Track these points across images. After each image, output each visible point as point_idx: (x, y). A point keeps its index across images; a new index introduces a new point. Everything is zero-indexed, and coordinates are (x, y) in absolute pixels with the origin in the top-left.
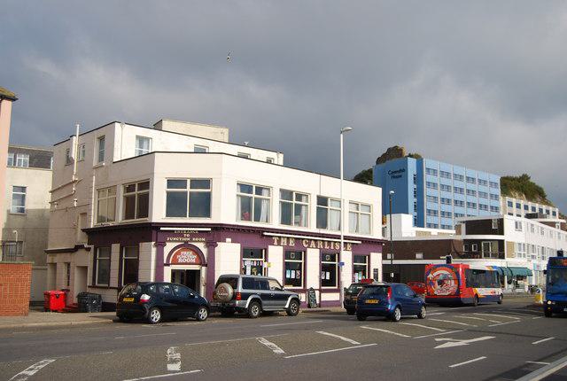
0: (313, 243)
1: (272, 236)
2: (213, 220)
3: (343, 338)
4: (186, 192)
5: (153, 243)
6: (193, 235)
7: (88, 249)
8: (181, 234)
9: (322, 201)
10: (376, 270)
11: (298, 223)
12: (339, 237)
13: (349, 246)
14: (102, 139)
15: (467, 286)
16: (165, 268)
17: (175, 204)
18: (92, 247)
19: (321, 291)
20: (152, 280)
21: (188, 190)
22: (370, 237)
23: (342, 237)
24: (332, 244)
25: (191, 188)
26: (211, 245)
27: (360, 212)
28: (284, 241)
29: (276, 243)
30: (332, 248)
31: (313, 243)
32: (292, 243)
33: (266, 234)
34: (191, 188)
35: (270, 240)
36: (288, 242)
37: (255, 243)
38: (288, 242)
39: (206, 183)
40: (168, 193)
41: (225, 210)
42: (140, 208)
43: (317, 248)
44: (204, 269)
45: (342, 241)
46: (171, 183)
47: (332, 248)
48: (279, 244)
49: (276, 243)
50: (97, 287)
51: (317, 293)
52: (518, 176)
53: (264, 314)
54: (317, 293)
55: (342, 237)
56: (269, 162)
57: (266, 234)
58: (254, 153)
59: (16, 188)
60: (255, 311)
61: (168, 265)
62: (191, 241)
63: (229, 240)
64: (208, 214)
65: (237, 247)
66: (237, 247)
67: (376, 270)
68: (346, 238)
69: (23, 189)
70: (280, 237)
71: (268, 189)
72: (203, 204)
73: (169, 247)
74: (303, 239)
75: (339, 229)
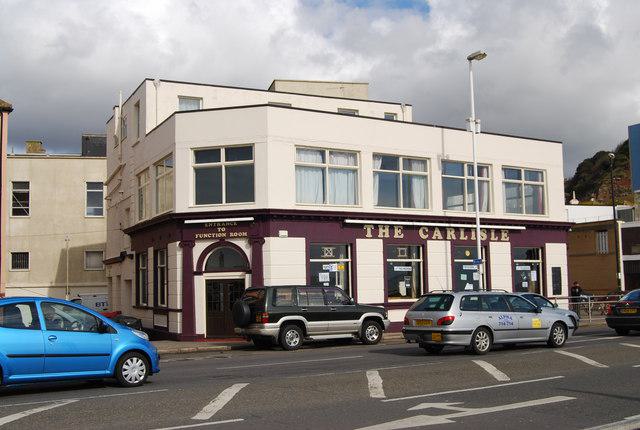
0: (437, 233)
1: (362, 225)
2: (258, 204)
4: (463, 180)
5: (178, 243)
6: (230, 227)
7: (131, 256)
8: (213, 228)
9: (447, 165)
10: (557, 272)
11: (409, 203)
12: (472, 221)
13: (504, 235)
14: (137, 105)
16: (196, 277)
17: (206, 186)
18: (134, 253)
20: (179, 307)
21: (223, 162)
22: (547, 220)
23: (478, 221)
25: (227, 160)
26: (257, 243)
27: (327, 165)
28: (451, 234)
29: (369, 234)
31: (437, 233)
32: (398, 234)
33: (348, 221)
34: (227, 160)
35: (360, 231)
36: (458, 236)
38: (458, 236)
39: (246, 151)
40: (197, 170)
41: (277, 190)
42: (471, 223)
43: (445, 239)
44: (248, 278)
45: (478, 226)
46: (202, 155)
47: (462, 238)
48: (375, 235)
49: (369, 234)
53: (308, 344)
55: (478, 221)
56: (389, 118)
57: (348, 221)
58: (363, 108)
59: (90, 185)
60: (293, 339)
61: (199, 273)
62: (228, 237)
64: (252, 199)
65: (301, 242)
66: (301, 242)
67: (557, 272)
68: (484, 221)
69: (26, 185)
70: (376, 226)
71: (487, 168)
72: (243, 182)
73: (199, 248)
74: (420, 227)
75: (488, 210)
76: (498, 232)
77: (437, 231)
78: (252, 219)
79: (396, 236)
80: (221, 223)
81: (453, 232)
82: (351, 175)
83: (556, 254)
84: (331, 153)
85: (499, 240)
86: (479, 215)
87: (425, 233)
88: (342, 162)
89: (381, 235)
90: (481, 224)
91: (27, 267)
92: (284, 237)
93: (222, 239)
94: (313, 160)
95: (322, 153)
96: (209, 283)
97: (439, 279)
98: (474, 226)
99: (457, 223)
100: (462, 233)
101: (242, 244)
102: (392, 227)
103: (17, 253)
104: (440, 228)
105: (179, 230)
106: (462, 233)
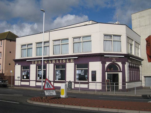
0: (50, 62)
3: (133, 74)
12: (41, 58)
15: (29, 81)
19: (75, 83)
23: (43, 58)
24: (61, 61)
28: (54, 62)
29: (33, 63)
30: (61, 62)
31: (50, 62)
35: (31, 63)
36: (38, 62)
37: (25, 64)
38: (38, 62)
47: (57, 62)
48: (34, 64)
49: (33, 63)
50: (61, 65)
51: (73, 83)
52: (101, 65)
54: (73, 83)
55: (43, 58)
63: (17, 64)
64: (32, 56)
65: (20, 66)
66: (20, 66)
68: (44, 58)
70: (35, 61)
76: (69, 60)
77: (50, 61)
78: (124, 56)
79: (39, 63)
80: (114, 57)
81: (37, 62)
82: (119, 42)
83: (95, 66)
84: (113, 36)
85: (70, 62)
86: (43, 56)
87: (46, 62)
88: (116, 38)
89: (35, 63)
90: (44, 59)
91: (92, 71)
92: (17, 65)
93: (113, 62)
94: (108, 38)
95: (111, 36)
96: (23, 79)
97: (50, 76)
98: (42, 60)
99: (55, 58)
100: (57, 61)
101: (120, 64)
102: (38, 61)
103: (96, 73)
104: (50, 60)
105: (4, 73)
106: (57, 61)
